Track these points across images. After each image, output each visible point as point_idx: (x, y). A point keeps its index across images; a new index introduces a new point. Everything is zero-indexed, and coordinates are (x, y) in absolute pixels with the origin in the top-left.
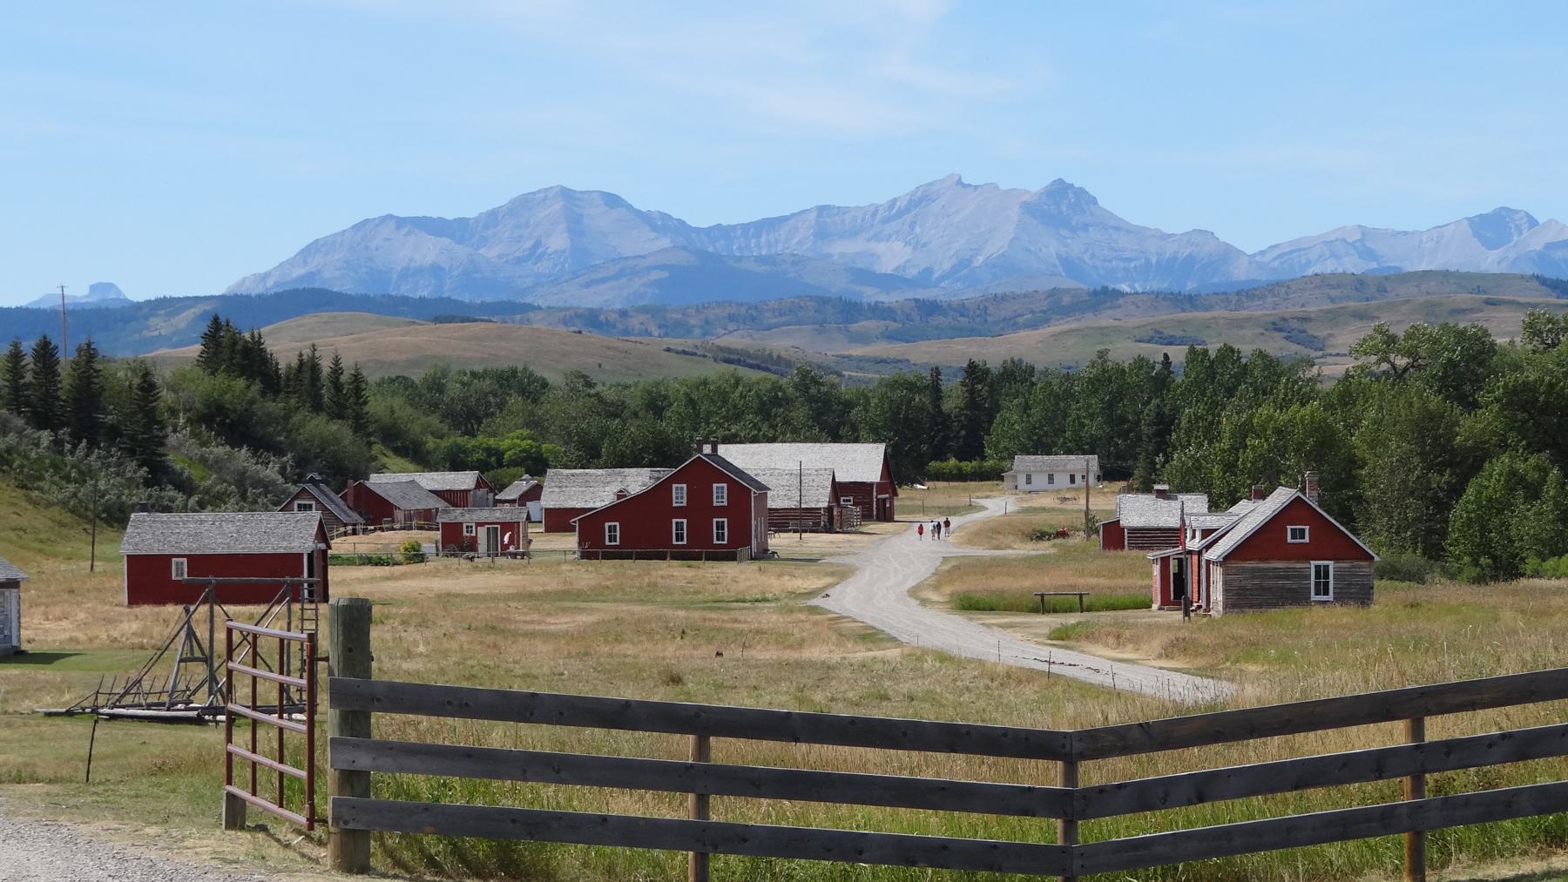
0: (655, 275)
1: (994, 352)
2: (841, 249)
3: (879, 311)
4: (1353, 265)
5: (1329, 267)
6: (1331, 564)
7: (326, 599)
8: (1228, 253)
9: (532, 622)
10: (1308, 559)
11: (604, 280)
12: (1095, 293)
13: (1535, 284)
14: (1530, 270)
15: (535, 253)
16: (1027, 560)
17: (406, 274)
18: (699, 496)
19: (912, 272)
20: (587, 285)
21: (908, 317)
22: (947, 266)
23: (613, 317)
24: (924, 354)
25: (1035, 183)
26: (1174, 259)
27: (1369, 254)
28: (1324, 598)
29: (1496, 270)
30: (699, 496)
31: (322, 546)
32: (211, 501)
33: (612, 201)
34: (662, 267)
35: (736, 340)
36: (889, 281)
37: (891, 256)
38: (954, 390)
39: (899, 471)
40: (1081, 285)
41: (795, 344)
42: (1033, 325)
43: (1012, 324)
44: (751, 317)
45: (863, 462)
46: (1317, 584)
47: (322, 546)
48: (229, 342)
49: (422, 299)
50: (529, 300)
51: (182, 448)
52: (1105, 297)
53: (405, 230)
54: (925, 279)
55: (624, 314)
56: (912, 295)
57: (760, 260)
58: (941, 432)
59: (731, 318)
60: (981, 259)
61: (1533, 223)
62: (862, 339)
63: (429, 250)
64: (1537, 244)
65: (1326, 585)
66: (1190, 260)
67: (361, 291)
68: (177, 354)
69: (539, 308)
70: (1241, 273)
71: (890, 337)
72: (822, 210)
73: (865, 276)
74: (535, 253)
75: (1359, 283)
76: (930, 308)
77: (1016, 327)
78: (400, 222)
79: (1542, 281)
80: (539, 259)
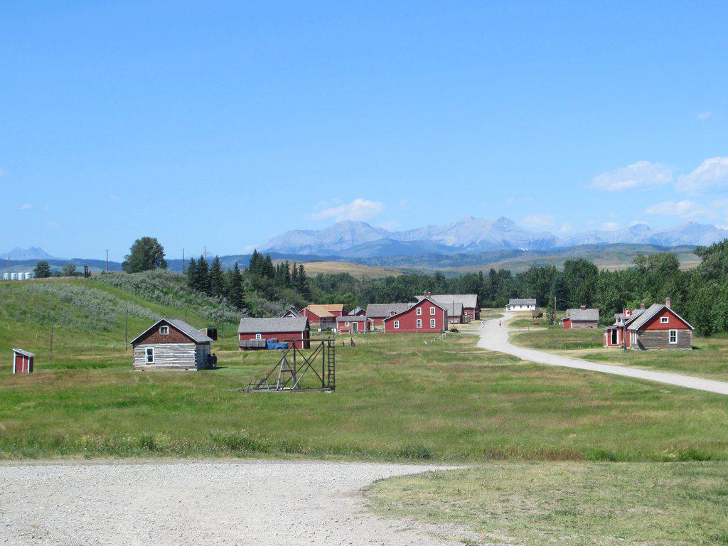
0: (378, 247)
1: (497, 267)
2: (434, 238)
3: (447, 257)
4: (592, 241)
5: (586, 242)
6: (676, 330)
7: (208, 343)
8: (553, 239)
9: (114, 350)
10: (668, 329)
11: (362, 249)
12: (515, 251)
13: (650, 247)
14: (648, 243)
15: (341, 241)
16: (538, 332)
17: (302, 248)
18: (426, 312)
19: (457, 246)
20: (357, 251)
21: (457, 259)
22: (468, 243)
23: (366, 260)
24: (475, 270)
25: (120, 252)
26: (538, 241)
27: (599, 239)
28: (673, 343)
29: (637, 243)
30: (426, 312)
31: (308, 329)
32: (261, 315)
33: (365, 224)
34: (381, 245)
35: (406, 266)
36: (452, 248)
37: (450, 240)
38: (487, 279)
39: (480, 305)
40: (508, 249)
41: (429, 270)
42: (496, 261)
43: (490, 261)
44: (408, 260)
45: (471, 301)
46: (672, 338)
47: (308, 329)
48: (260, 263)
49: (307, 255)
50: (339, 255)
51: (251, 298)
52: (517, 252)
53: (300, 235)
54: (461, 247)
55: (369, 259)
56: (458, 252)
57: (410, 242)
58: (491, 291)
59: (402, 260)
60: (479, 241)
61: (648, 228)
62: (444, 266)
63: (308, 240)
64: (649, 235)
65: (672, 335)
66: (543, 241)
67: (287, 253)
68: (315, 276)
69: (343, 258)
70: (558, 245)
71: (452, 265)
72: (428, 226)
73: (444, 247)
74: (341, 241)
75: (597, 246)
76: (463, 256)
77: (490, 262)
78: (299, 232)
79: (653, 246)
80: (342, 242)
